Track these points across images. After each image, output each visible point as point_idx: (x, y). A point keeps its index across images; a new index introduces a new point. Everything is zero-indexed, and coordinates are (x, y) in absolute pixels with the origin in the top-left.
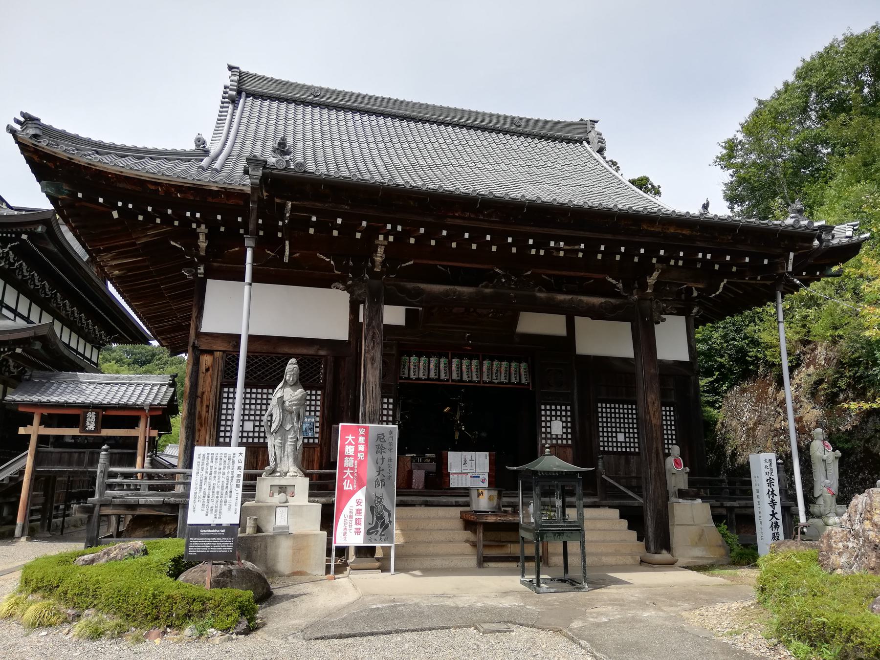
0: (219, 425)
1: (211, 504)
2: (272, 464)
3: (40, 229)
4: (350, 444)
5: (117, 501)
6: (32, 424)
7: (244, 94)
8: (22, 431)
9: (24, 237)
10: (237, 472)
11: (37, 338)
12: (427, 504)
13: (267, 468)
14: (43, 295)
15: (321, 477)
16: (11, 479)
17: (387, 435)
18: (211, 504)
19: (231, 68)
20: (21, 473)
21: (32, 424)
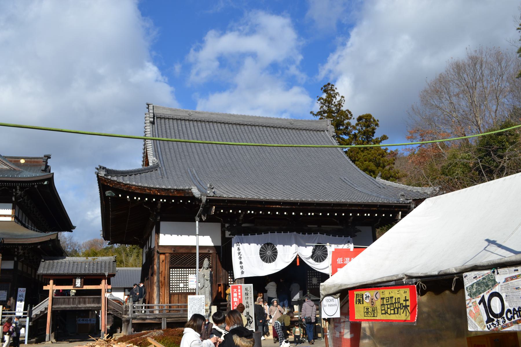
0: (170, 285)
3: (46, 183)
4: (235, 292)
6: (49, 284)
8: (45, 288)
10: (202, 304)
17: (248, 289)
20: (46, 309)
21: (49, 284)
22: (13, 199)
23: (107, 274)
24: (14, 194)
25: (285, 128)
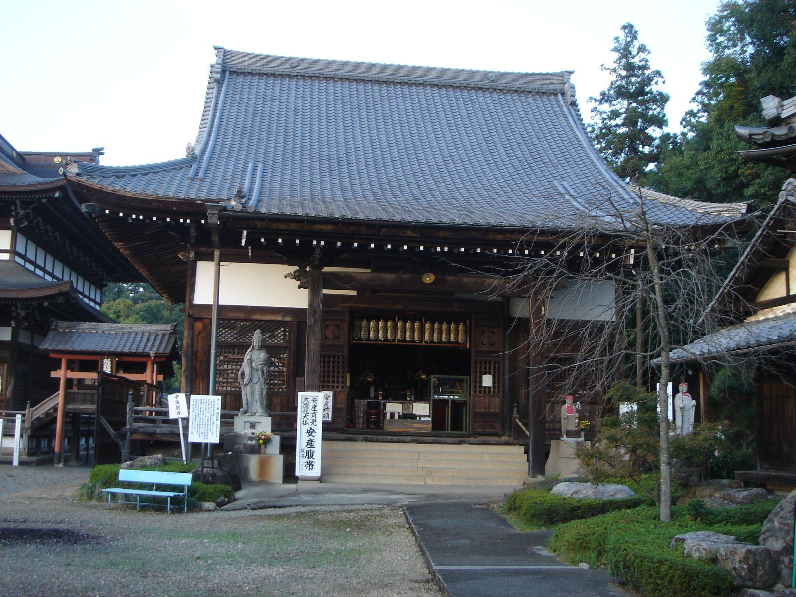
1: (202, 431)
2: (245, 407)
3: (57, 195)
5: (142, 430)
7: (228, 73)
8: (53, 374)
9: (44, 201)
10: (216, 411)
11: (61, 294)
12: (367, 440)
13: (241, 410)
14: (55, 245)
15: (282, 417)
16: (47, 414)
18: (202, 431)
19: (216, 49)
20: (55, 409)
22: (12, 221)
23: (152, 354)
24: (14, 213)
25: (424, 85)
